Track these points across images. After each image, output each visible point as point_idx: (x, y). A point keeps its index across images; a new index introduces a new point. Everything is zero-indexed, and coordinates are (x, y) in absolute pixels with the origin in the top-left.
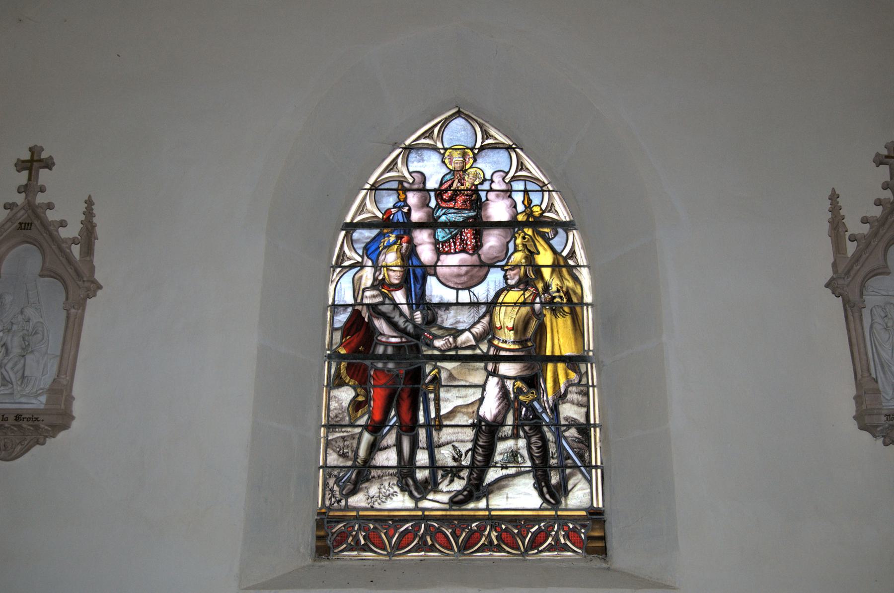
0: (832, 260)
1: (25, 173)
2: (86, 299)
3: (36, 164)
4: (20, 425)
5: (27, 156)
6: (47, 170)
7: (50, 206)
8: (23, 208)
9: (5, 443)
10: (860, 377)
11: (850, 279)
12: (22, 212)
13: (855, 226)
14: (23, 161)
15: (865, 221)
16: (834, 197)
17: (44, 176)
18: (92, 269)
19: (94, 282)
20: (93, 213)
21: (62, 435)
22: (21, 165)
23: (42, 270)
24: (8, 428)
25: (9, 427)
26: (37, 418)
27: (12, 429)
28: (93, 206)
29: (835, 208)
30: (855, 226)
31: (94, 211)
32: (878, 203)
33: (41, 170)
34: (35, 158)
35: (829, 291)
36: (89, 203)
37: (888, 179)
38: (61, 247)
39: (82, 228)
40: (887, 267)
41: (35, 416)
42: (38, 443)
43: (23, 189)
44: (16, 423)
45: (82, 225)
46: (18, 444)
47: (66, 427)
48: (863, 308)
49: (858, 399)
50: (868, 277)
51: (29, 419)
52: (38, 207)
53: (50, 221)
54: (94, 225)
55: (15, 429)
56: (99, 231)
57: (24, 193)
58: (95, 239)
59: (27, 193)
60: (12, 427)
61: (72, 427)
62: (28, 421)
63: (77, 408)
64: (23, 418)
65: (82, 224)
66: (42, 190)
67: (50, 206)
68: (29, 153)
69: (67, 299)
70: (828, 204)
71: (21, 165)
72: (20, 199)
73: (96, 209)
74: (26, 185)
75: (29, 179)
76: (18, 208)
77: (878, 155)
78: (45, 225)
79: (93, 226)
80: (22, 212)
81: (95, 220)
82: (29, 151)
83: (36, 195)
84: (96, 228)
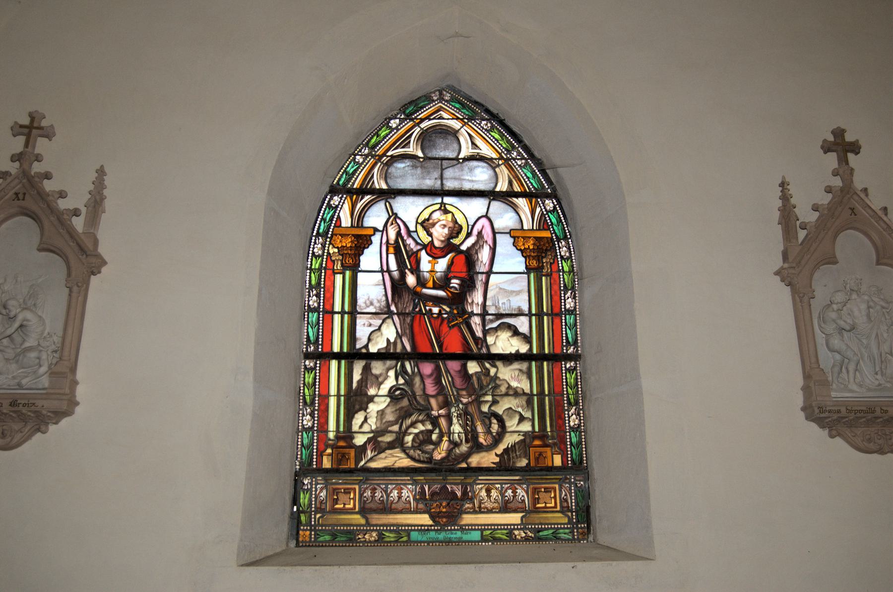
0: (781, 248)
1: (22, 139)
2: (89, 277)
3: (34, 131)
4: (19, 411)
5: (26, 121)
6: (846, 134)
7: (48, 176)
8: (17, 177)
9: (3, 430)
10: (809, 368)
11: (800, 268)
12: (17, 181)
13: (806, 214)
14: (21, 126)
15: (815, 208)
16: (783, 185)
17: (41, 145)
18: (96, 242)
19: (99, 256)
20: (104, 183)
21: (65, 422)
22: (18, 130)
23: (41, 243)
24: (6, 414)
25: (7, 414)
26: (34, 404)
27: (11, 416)
28: (104, 177)
29: (785, 197)
30: (806, 214)
31: (105, 183)
32: (829, 190)
33: (39, 139)
34: (35, 125)
35: (778, 278)
36: (101, 172)
37: (837, 166)
38: (62, 220)
39: (89, 199)
40: (835, 257)
41: (31, 401)
42: (39, 430)
43: (17, 158)
44: (13, 409)
45: (90, 196)
46: (17, 431)
47: (68, 413)
48: (812, 298)
49: (806, 389)
50: (822, 263)
51: (25, 405)
52: (33, 177)
53: (48, 191)
54: (104, 197)
55: (14, 415)
56: (107, 204)
57: (18, 162)
58: (102, 213)
59: (22, 161)
60: (11, 413)
61: (75, 412)
62: (23, 406)
63: (81, 392)
64: (19, 404)
65: (90, 194)
66: (38, 158)
67: (48, 176)
68: (29, 119)
69: (69, 274)
70: (778, 191)
71: (18, 130)
72: (13, 168)
73: (108, 180)
74: (21, 153)
75: (27, 145)
76: (12, 178)
77: (825, 141)
78: (42, 195)
79: (103, 198)
80: (17, 181)
81: (105, 192)
82: (29, 116)
83: (31, 164)
84: (106, 200)
